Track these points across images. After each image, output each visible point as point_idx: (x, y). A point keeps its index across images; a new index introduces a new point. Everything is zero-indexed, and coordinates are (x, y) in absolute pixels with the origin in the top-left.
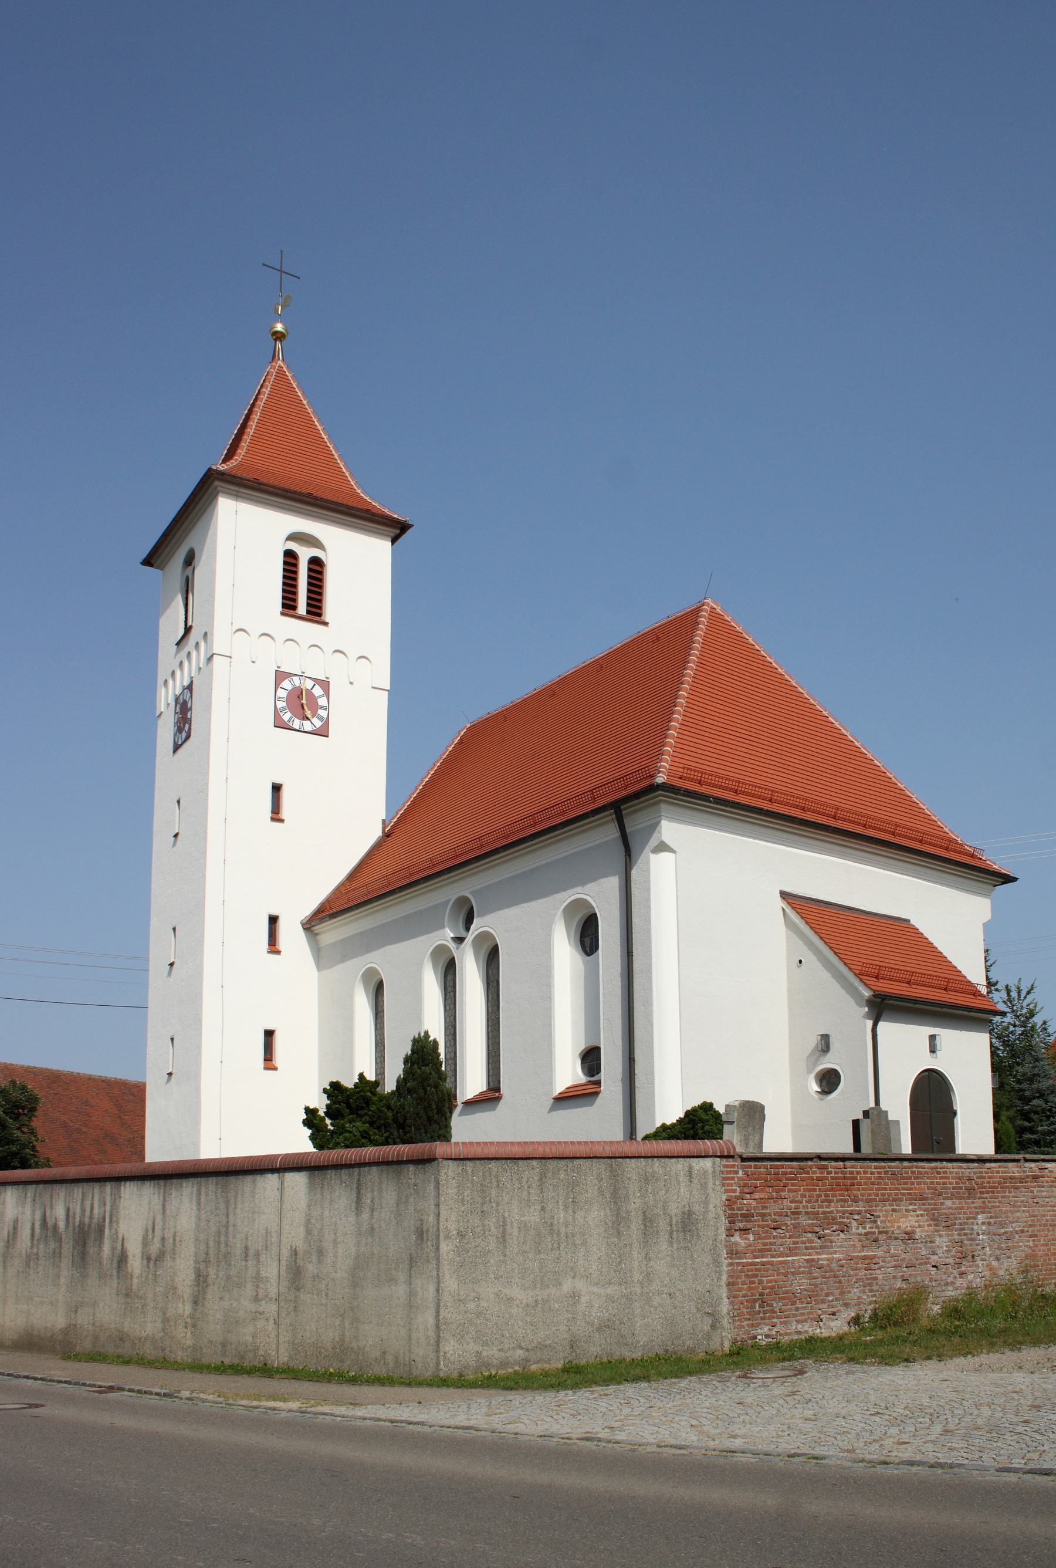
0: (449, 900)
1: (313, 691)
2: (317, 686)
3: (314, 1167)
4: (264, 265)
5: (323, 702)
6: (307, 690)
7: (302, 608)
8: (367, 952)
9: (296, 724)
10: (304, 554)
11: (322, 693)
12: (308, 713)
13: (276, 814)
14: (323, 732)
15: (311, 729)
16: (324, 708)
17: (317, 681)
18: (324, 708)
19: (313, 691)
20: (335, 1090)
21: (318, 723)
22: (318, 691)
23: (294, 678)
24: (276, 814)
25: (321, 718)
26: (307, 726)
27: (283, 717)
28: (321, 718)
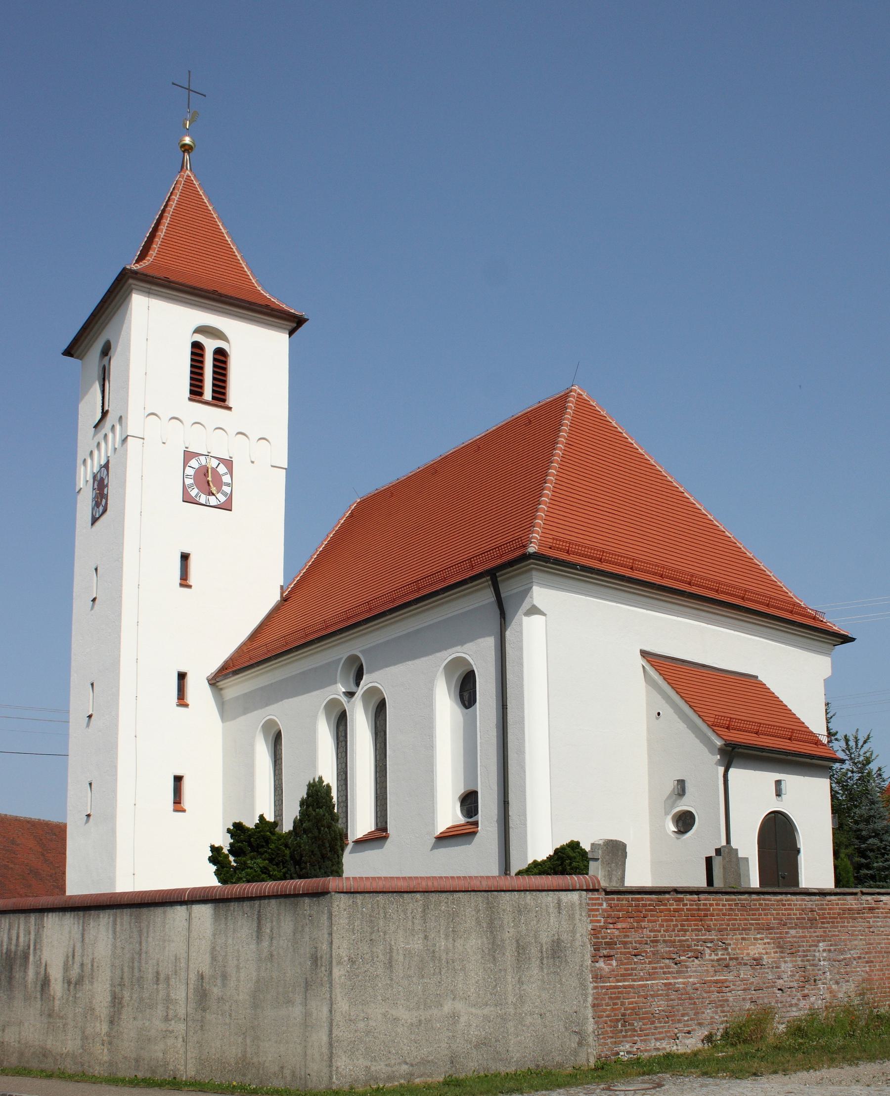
0: (342, 658)
1: (218, 469)
2: (221, 465)
5: (226, 479)
7: (208, 394)
14: (227, 506)
16: (228, 485)
18: (228, 485)
21: (222, 499)
22: (222, 469)
25: (225, 494)
28: (225, 494)
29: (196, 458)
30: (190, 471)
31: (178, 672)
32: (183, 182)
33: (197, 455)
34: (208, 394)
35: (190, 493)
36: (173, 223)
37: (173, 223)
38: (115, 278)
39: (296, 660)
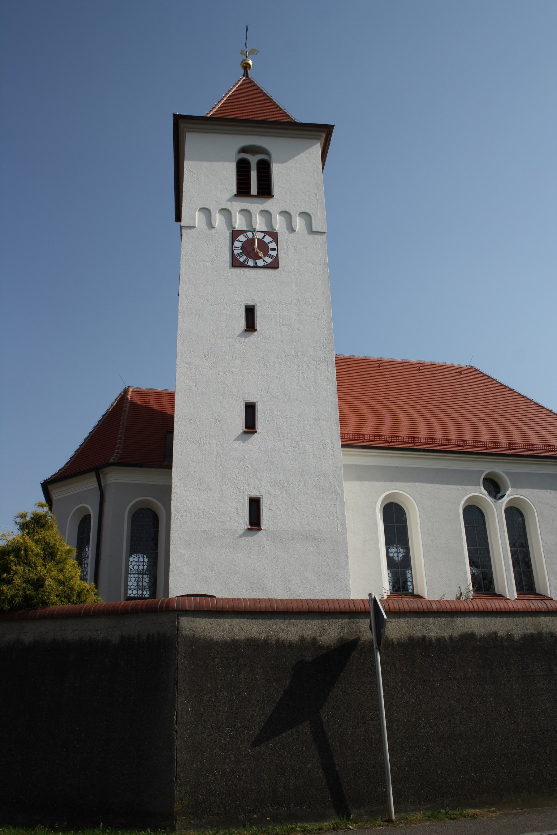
0: (483, 471)
1: (264, 240)
2: (267, 236)
3: (194, 611)
4: (120, 375)
5: (273, 245)
6: (258, 239)
7: (254, 190)
8: (392, 481)
9: (251, 263)
10: (253, 160)
11: (271, 239)
12: (261, 254)
13: (250, 311)
14: (274, 265)
15: (264, 265)
16: (273, 249)
17: (243, 265)
18: (273, 249)
19: (264, 240)
20: (314, 639)
21: (269, 260)
22: (268, 239)
23: (247, 233)
24: (250, 311)
25: (271, 256)
26: (260, 263)
27: (240, 259)
28: (271, 256)
29: (244, 234)
30: (237, 244)
31: (250, 498)
32: (122, 448)
33: (267, 267)
34: (254, 190)
35: (239, 259)
36: (133, 398)
37: (133, 398)
38: (532, 566)
39: (402, 457)
